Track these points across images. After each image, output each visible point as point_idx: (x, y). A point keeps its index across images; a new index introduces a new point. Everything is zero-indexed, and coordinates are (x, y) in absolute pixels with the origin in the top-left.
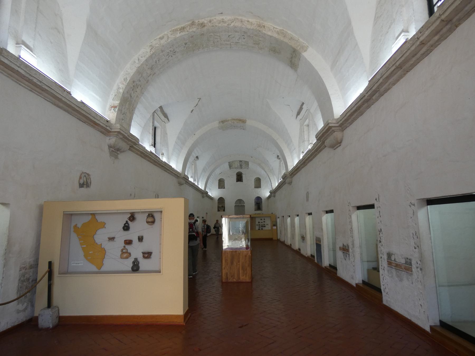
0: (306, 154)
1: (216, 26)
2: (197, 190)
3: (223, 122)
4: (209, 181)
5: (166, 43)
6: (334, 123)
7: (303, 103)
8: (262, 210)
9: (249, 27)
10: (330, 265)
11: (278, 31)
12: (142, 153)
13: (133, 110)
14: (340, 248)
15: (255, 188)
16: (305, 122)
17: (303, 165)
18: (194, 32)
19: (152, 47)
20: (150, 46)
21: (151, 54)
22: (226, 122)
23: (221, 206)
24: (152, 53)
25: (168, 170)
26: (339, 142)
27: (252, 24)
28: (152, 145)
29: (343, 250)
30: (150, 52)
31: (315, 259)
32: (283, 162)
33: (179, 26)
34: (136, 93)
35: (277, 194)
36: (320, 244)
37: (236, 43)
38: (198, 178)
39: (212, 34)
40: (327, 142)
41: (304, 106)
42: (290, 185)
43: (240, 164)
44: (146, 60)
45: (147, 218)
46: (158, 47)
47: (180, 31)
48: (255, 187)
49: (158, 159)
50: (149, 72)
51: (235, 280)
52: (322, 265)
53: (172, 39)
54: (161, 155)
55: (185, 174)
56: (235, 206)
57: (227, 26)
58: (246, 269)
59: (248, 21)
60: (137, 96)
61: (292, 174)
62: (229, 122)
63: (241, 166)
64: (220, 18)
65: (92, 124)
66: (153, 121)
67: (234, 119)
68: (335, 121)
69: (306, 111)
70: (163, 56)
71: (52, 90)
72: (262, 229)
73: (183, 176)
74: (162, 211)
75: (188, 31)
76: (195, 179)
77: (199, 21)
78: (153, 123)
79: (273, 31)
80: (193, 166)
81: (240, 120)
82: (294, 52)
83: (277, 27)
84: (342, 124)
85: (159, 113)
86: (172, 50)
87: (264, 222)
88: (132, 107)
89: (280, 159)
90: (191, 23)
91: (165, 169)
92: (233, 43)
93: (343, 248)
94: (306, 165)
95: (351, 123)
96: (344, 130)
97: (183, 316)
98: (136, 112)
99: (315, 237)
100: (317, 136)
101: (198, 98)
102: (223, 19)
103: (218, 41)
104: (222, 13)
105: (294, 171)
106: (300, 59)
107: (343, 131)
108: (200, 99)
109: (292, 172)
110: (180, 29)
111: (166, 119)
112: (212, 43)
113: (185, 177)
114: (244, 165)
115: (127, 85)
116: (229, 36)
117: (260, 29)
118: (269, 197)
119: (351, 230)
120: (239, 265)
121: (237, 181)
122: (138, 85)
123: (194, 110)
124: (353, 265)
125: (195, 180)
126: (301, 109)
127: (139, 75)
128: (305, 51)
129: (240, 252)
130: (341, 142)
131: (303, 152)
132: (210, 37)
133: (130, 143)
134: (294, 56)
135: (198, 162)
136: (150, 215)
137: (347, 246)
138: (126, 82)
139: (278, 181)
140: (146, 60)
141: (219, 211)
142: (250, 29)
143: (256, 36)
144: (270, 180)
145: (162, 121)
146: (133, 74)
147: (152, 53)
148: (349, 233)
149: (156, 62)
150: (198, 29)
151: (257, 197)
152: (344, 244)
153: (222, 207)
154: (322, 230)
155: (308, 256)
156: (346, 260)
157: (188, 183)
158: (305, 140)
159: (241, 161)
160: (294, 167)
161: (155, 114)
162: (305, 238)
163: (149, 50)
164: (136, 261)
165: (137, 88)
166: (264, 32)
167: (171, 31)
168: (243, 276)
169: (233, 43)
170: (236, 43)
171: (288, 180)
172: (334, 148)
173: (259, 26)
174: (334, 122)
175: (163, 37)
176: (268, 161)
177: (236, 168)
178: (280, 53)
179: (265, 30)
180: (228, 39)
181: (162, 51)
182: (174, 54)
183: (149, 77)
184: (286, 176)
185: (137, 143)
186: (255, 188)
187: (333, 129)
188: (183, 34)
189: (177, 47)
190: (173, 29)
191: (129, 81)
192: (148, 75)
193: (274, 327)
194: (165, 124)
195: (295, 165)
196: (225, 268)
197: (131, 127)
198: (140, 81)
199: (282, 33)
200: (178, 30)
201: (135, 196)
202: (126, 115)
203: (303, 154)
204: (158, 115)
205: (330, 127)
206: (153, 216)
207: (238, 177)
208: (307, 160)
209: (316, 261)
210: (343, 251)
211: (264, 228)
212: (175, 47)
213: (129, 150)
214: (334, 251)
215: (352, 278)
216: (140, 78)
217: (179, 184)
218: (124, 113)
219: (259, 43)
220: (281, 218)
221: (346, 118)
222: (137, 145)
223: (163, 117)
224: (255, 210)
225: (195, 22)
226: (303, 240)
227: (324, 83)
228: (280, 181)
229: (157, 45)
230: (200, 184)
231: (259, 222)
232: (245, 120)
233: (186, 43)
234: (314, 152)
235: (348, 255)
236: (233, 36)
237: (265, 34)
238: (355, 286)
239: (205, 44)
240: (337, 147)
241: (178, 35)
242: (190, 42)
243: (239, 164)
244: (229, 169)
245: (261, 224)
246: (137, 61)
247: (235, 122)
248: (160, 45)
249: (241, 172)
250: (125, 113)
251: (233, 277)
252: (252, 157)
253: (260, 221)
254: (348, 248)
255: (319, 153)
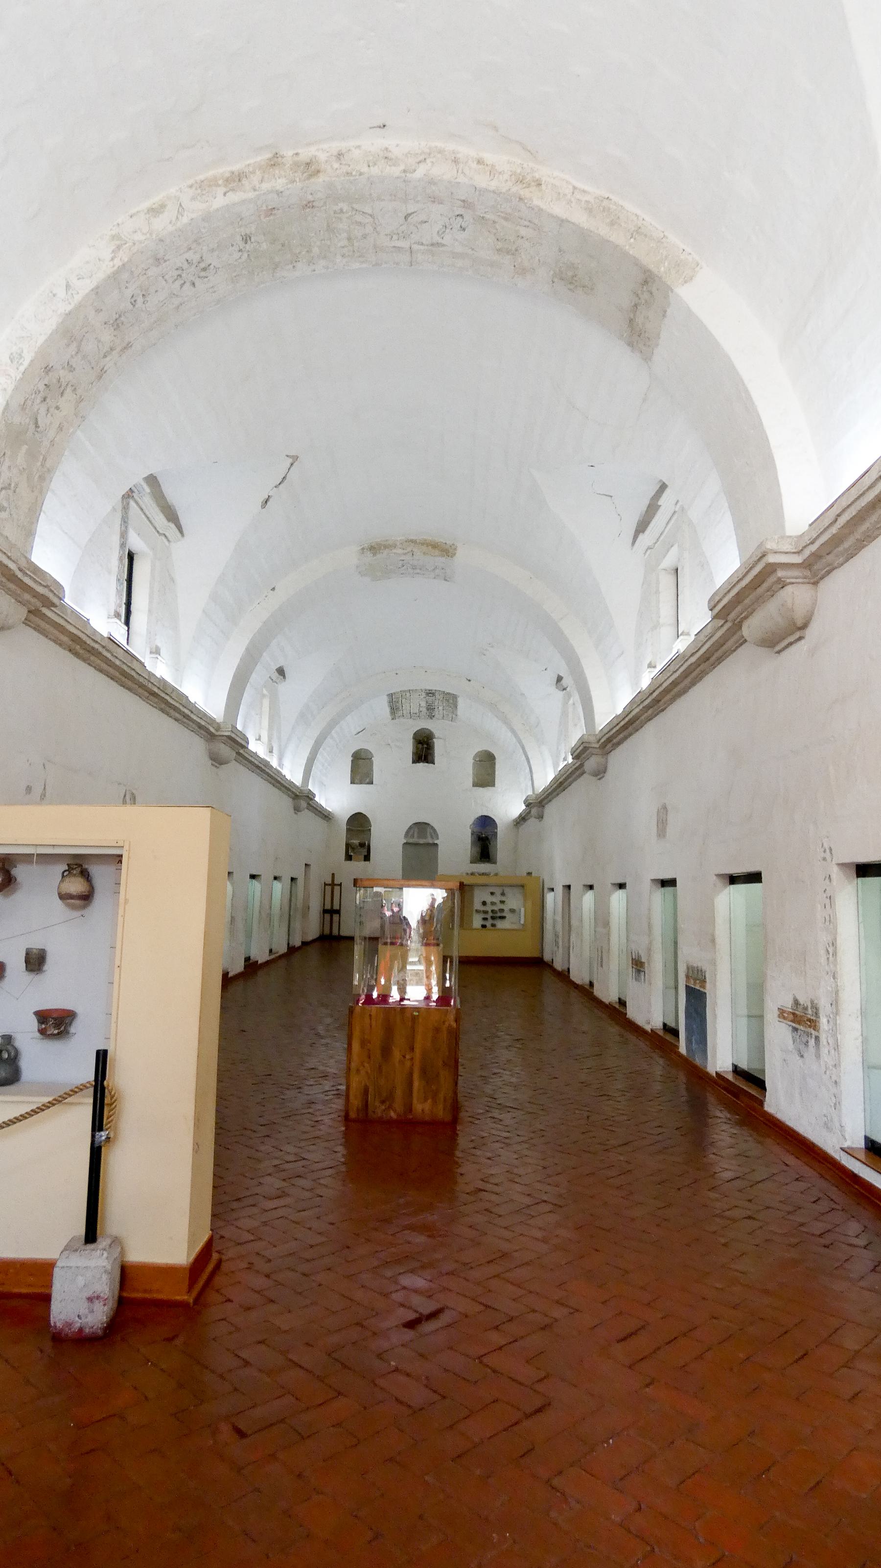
0: (662, 672)
1: (361, 174)
2: (278, 785)
3: (374, 549)
4: (319, 756)
5: (171, 228)
6: (787, 553)
7: (664, 483)
8: (495, 863)
9: (482, 181)
10: (736, 1070)
11: (587, 202)
12: (75, 639)
13: (42, 478)
14: (782, 1013)
15: (474, 786)
16: (664, 557)
17: (650, 712)
18: (279, 193)
19: (118, 242)
20: (113, 237)
21: (113, 266)
22: (386, 552)
23: (356, 842)
24: (118, 263)
25: (176, 709)
26: (799, 623)
27: (493, 171)
28: (117, 615)
29: (792, 1021)
30: (112, 259)
31: (678, 1041)
32: (576, 698)
33: (224, 170)
34: (56, 411)
35: (551, 810)
36: (702, 989)
37: (432, 245)
38: (280, 746)
39: (345, 206)
40: (752, 628)
41: (666, 502)
42: (600, 779)
43: (427, 702)
44: (97, 287)
45: (62, 881)
46: (141, 242)
47: (225, 186)
48: (476, 784)
49: (135, 665)
50: (107, 336)
51: (393, 1115)
52: (706, 1067)
53: (194, 216)
54: (151, 653)
55: (234, 727)
56: (405, 844)
57: (403, 175)
58: (438, 1075)
59: (480, 162)
60: (61, 428)
61: (609, 740)
62: (394, 551)
63: (430, 709)
64: (374, 143)
65: (273, 781)
66: (123, 528)
67: (412, 541)
68: (791, 544)
69: (668, 517)
70: (161, 278)
71: (69, 624)
72: (493, 925)
73: (227, 734)
74: (121, 856)
75: (257, 188)
76: (272, 748)
77: (297, 154)
78: (124, 535)
79: (569, 202)
80: (266, 703)
81: (435, 546)
82: (646, 282)
83: (586, 188)
84: (816, 556)
85: (147, 501)
86: (196, 258)
87: (502, 902)
88: (42, 465)
89: (564, 689)
90: (270, 160)
91: (163, 706)
92: (422, 247)
93: (794, 1014)
94: (663, 710)
95: (850, 555)
96: (822, 578)
97: (187, 1272)
98: (57, 482)
99: (685, 968)
100: (713, 604)
101: (287, 456)
102: (387, 149)
103: (365, 237)
104: (384, 126)
105: (614, 730)
106: (665, 312)
107: (815, 583)
108: (295, 458)
109: (607, 736)
110: (227, 181)
111: (173, 526)
112: (346, 242)
113: (233, 736)
114: (441, 708)
115: (21, 379)
116: (406, 218)
117: (522, 193)
118: (522, 819)
119: (831, 950)
120: (412, 1059)
121: (414, 762)
122: (64, 384)
123: (271, 500)
124: (834, 1078)
125: (271, 752)
126: (652, 508)
127: (68, 345)
128: (686, 282)
129: (416, 1014)
130: (804, 626)
131: (651, 666)
132: (338, 215)
133: (27, 596)
134: (646, 301)
135: (284, 688)
136: (73, 869)
137: (812, 1007)
138: (18, 369)
139: (555, 765)
140: (96, 291)
141: (349, 858)
142: (486, 190)
143: (506, 219)
144: (528, 762)
145: (158, 532)
146: (46, 341)
147: (120, 264)
148: (823, 960)
149: (134, 304)
150: (293, 181)
151: (482, 816)
152: (798, 998)
153: (362, 845)
154: (713, 941)
155: (652, 1030)
156: (802, 1056)
157: (246, 759)
158: (661, 621)
159: (430, 693)
160: (617, 717)
161: (132, 503)
162: (646, 965)
163: (107, 254)
164: (9, 1047)
165: (62, 394)
166: (536, 202)
167: (191, 187)
168: (426, 1100)
169: (422, 244)
170: (432, 245)
171: (591, 763)
172: (778, 648)
173: (520, 180)
174: (787, 547)
175: (163, 206)
176: (523, 694)
177: (411, 716)
178: (592, 289)
179: (542, 198)
180: (404, 228)
181: (158, 261)
182: (203, 274)
183: (105, 356)
184: (585, 749)
185: (55, 600)
186: (474, 786)
187: (780, 573)
188: (234, 197)
189: (213, 250)
190: (201, 177)
191: (30, 365)
192: (104, 351)
193: (543, 1329)
194: (167, 543)
195: (619, 711)
196: (358, 1071)
197: (37, 540)
198: (71, 369)
199: (604, 210)
200: (220, 182)
201: (43, 796)
202: (15, 492)
203: (652, 669)
204: (142, 509)
205: (771, 569)
206: (85, 875)
207: (420, 746)
208: (667, 691)
209: (683, 1049)
210: (794, 1025)
211: (500, 924)
212: (204, 248)
213: (23, 623)
214: (757, 1018)
215: (827, 1126)
216: (72, 356)
217: (210, 762)
218: (10, 485)
219: (516, 250)
220: (559, 890)
221: (834, 530)
222: (54, 605)
223: (160, 519)
224: (473, 862)
225: (282, 157)
226: (639, 971)
227: (753, 403)
228: (562, 765)
229: (139, 237)
230: (287, 762)
231: (484, 903)
232: (453, 544)
233: (246, 235)
234: (697, 664)
235: (812, 1042)
236: (423, 217)
237: (540, 210)
238: (714, 1075)
239: (318, 243)
240: (791, 644)
241: (219, 200)
242: (264, 234)
243: (423, 704)
244: (390, 717)
245: (489, 908)
246: (61, 293)
247: (415, 550)
248: (148, 235)
249: (430, 730)
250: (13, 485)
251: (388, 1103)
252: (469, 680)
253: (489, 899)
254: (817, 1014)
255: (714, 666)
